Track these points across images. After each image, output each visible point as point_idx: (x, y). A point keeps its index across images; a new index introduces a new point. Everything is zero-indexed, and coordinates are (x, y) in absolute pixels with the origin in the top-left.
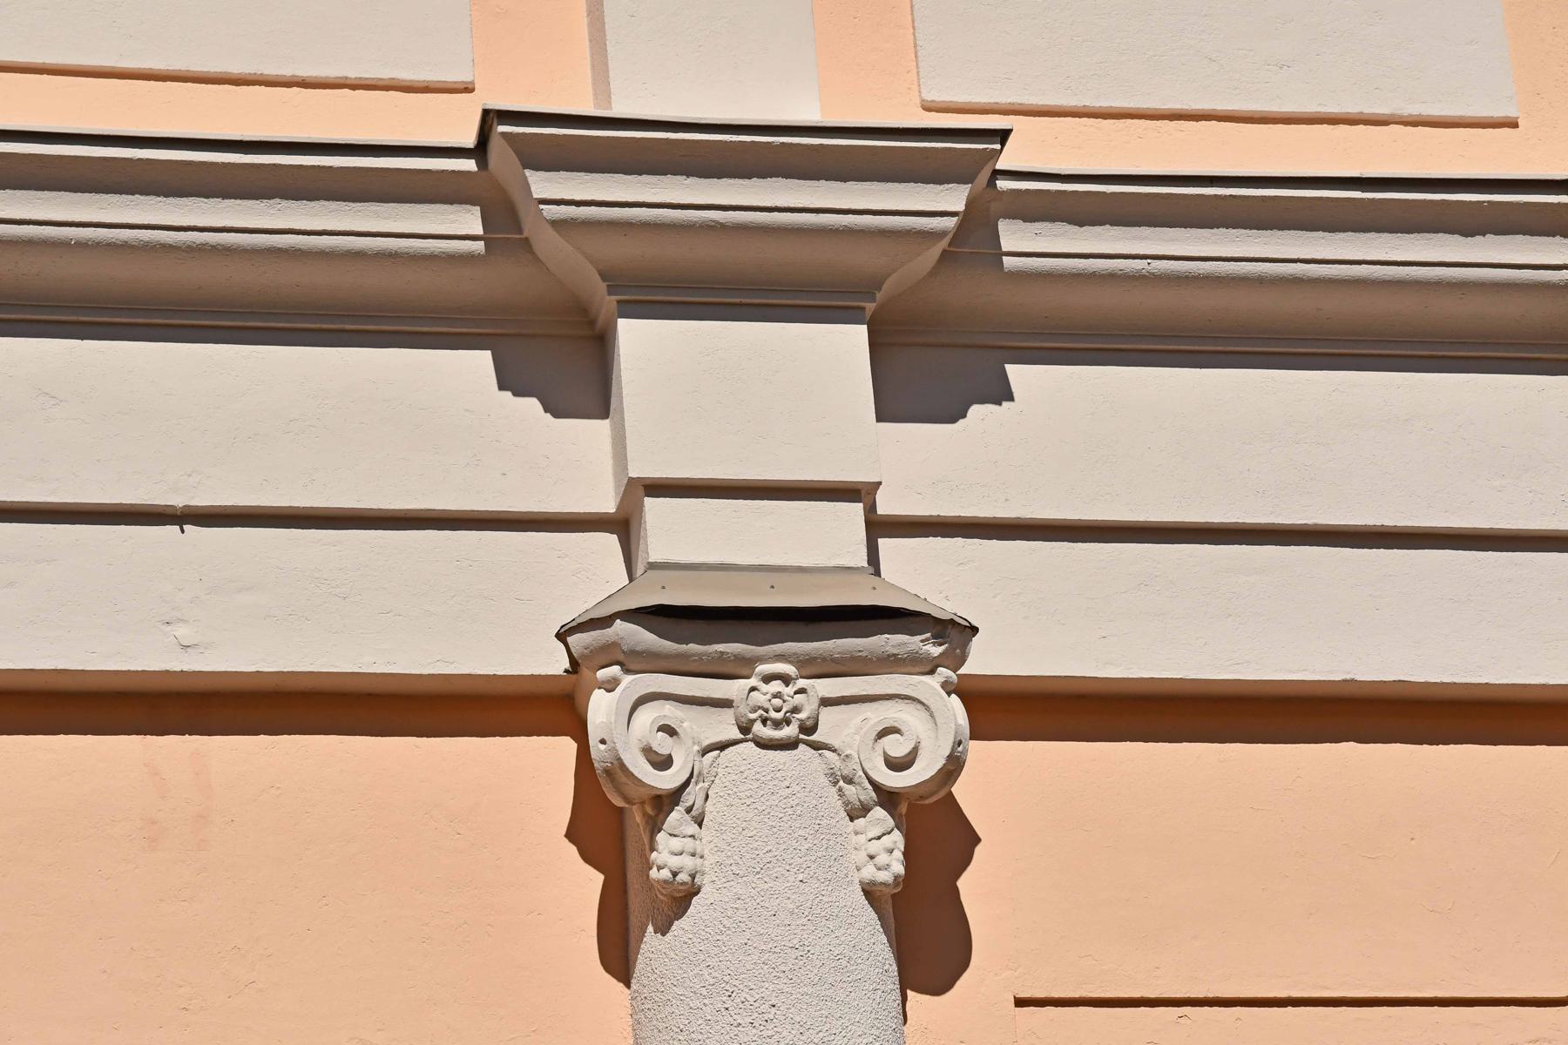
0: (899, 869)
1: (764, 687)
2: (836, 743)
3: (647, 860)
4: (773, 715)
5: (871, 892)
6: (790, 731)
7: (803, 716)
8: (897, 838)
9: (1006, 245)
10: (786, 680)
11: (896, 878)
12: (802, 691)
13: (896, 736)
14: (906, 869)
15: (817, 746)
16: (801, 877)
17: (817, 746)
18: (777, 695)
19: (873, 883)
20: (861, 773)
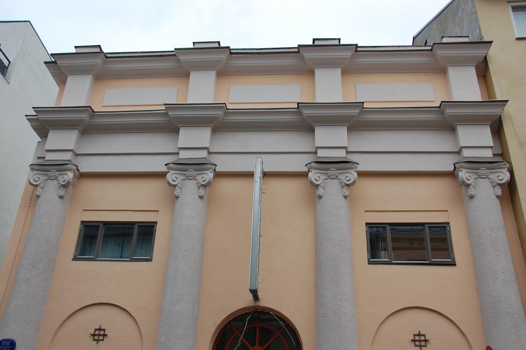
0: (501, 193)
2: (491, 178)
3: (467, 192)
4: (190, 176)
5: (498, 197)
6: (335, 177)
8: (500, 190)
9: (169, 114)
10: (54, 172)
11: (501, 195)
14: (502, 193)
15: (196, 180)
18: (333, 172)
19: (345, 196)
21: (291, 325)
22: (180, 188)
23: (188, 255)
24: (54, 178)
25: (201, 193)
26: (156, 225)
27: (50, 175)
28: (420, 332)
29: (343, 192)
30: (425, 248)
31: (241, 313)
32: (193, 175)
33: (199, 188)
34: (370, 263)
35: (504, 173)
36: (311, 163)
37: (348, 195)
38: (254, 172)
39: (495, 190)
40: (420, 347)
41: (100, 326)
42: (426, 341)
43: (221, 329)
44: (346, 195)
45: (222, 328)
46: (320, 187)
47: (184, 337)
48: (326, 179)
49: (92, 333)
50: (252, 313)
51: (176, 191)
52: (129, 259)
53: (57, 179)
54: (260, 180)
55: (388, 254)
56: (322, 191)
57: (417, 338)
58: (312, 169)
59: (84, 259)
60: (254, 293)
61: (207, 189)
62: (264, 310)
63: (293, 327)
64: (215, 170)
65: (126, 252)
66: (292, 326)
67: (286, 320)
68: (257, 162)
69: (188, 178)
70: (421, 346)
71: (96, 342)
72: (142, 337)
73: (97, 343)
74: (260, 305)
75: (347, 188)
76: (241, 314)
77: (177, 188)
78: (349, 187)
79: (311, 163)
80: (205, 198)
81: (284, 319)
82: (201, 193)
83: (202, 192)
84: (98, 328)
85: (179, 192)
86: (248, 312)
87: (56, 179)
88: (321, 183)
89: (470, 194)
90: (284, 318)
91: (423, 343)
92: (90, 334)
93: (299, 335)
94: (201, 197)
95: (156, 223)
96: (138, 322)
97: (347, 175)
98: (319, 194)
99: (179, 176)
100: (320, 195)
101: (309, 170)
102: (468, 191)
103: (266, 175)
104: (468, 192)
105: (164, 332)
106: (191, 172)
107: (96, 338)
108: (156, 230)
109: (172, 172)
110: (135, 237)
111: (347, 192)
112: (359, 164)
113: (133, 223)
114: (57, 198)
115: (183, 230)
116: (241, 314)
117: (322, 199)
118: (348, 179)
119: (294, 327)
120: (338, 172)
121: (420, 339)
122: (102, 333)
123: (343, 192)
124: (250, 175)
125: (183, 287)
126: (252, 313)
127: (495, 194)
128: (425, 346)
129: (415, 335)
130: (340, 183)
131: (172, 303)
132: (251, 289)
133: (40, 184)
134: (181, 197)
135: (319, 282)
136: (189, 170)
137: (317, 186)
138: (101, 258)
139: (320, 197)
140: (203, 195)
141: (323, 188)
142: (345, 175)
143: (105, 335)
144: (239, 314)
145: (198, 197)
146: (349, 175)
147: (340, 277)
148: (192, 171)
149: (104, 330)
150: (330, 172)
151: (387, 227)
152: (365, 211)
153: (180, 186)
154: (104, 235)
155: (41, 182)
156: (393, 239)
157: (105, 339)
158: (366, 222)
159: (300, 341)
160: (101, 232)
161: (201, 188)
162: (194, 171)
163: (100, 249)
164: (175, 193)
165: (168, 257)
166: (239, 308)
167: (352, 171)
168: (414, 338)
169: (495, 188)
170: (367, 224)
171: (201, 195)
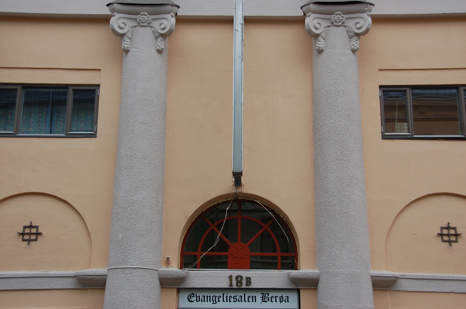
1: (336, 16)
2: (154, 26)
6: (341, 23)
7: (342, 21)
12: (148, 17)
13: (359, 24)
15: (151, 27)
16: (341, 48)
17: (151, 27)
18: (338, 17)
19: (354, 49)
20: (352, 31)
21: (281, 216)
22: (130, 39)
23: (147, 128)
24: (147, 24)
25: (160, 45)
26: (99, 89)
27: (140, 20)
28: (449, 224)
29: (352, 45)
30: (458, 118)
31: (217, 202)
32: (147, 21)
33: (156, 38)
34: (384, 137)
35: (167, 19)
36: (309, 4)
37: (358, 48)
38: (233, 16)
39: (352, 42)
40: (450, 242)
41: (31, 223)
42: (457, 235)
43: (192, 222)
44: (356, 48)
45: (193, 221)
46: (320, 38)
47: (148, 233)
48: (329, 26)
49: (21, 232)
50: (231, 201)
51: (125, 43)
52: (64, 135)
53: (151, 25)
54: (242, 28)
55: (408, 126)
56: (323, 43)
57: (445, 232)
58: (310, 13)
59: (7, 136)
60: (237, 176)
61: (166, 40)
62: (246, 197)
63: (284, 219)
64: (176, 14)
65: (58, 126)
66: (284, 218)
67: (275, 211)
68: (237, 3)
69: (140, 24)
70: (450, 241)
71: (26, 243)
72: (89, 235)
73: (28, 244)
74: (242, 192)
75: (162, 39)
76: (217, 204)
77: (125, 38)
78: (359, 38)
79: (309, 4)
80: (165, 53)
81: (272, 208)
82: (160, 45)
83: (161, 44)
84: (28, 224)
85: (129, 43)
86: (226, 201)
87: (343, 25)
88: (322, 32)
89: (318, 48)
90: (272, 207)
91: (453, 238)
92: (18, 233)
93: (293, 228)
94: (160, 52)
95: (98, 86)
96: (83, 217)
97: (358, 20)
98: (319, 48)
99: (127, 21)
100: (321, 48)
101: (305, 14)
102: (317, 44)
103: (248, 21)
104: (316, 45)
105: (121, 228)
106: (144, 16)
107: (26, 237)
108: (99, 96)
109: (117, 15)
110: (70, 106)
111: (356, 44)
112: (374, 5)
113: (66, 87)
114: (350, 52)
115: (138, 96)
116: (217, 204)
117: (324, 54)
118: (358, 26)
119: (285, 219)
120: (346, 16)
121: (449, 232)
122: (34, 231)
123: (351, 44)
124: (229, 21)
125: (142, 170)
126: (231, 201)
127: (351, 47)
128: (456, 241)
129: (442, 228)
130: (348, 32)
131: (129, 191)
132: (234, 172)
133: (128, 33)
134: (132, 50)
135: (319, 162)
136: (141, 13)
137: (317, 36)
138: (23, 133)
139: (320, 51)
140: (163, 49)
141: (324, 39)
142: (355, 21)
143: (38, 234)
144: (214, 204)
145: (156, 51)
146: (359, 20)
147: (348, 156)
148: (145, 15)
149: (37, 227)
150: (334, 16)
151: (408, 91)
152: (379, 70)
153: (130, 36)
154: (24, 103)
155: (128, 31)
156: (415, 108)
157: (39, 238)
158: (380, 85)
159: (293, 236)
160: (20, 99)
161: (160, 38)
162: (149, 15)
163: (21, 120)
164: (123, 45)
165: (119, 131)
166: (216, 196)
167: (365, 15)
168: (442, 231)
169: (352, 39)
170: (381, 87)
171: (159, 48)
